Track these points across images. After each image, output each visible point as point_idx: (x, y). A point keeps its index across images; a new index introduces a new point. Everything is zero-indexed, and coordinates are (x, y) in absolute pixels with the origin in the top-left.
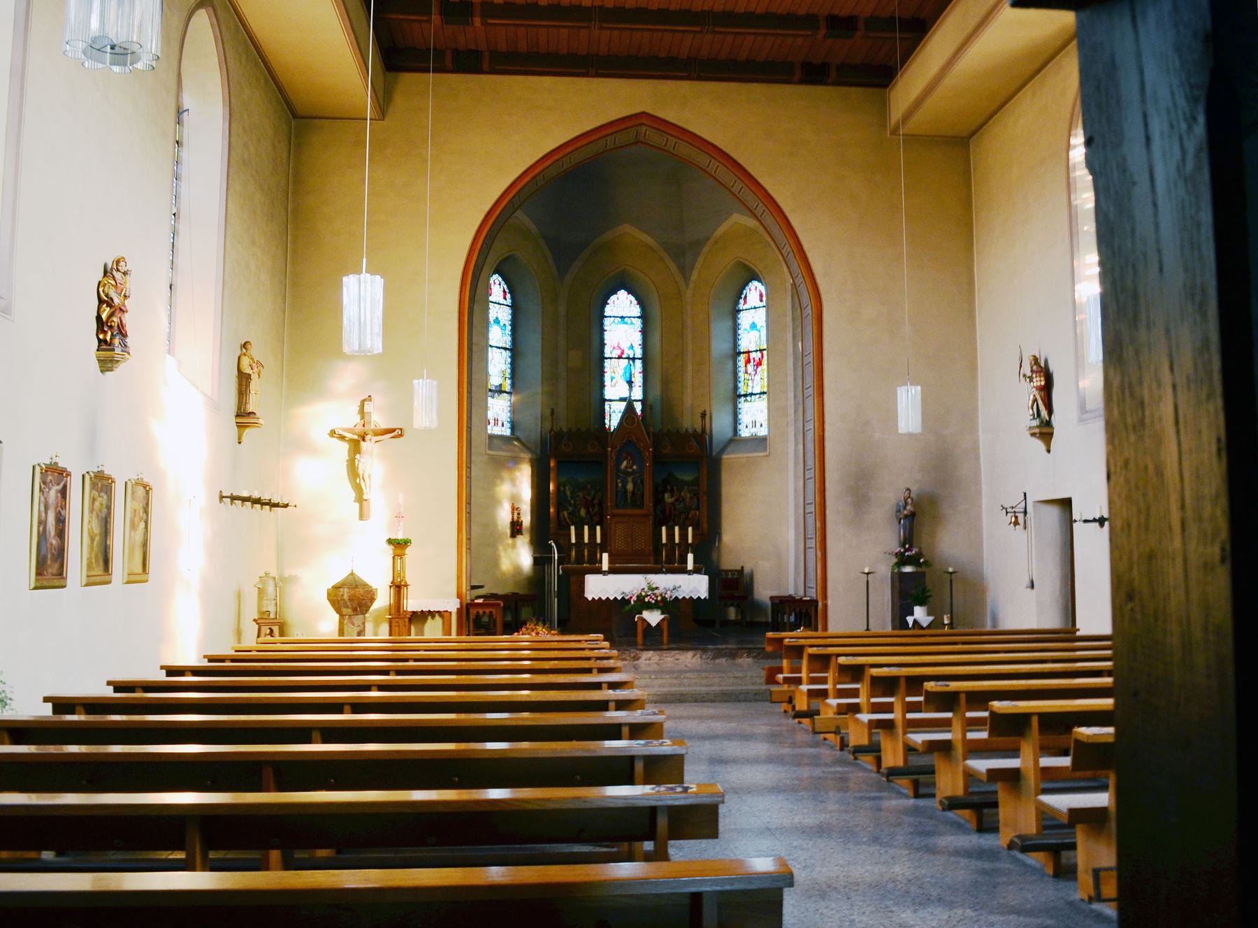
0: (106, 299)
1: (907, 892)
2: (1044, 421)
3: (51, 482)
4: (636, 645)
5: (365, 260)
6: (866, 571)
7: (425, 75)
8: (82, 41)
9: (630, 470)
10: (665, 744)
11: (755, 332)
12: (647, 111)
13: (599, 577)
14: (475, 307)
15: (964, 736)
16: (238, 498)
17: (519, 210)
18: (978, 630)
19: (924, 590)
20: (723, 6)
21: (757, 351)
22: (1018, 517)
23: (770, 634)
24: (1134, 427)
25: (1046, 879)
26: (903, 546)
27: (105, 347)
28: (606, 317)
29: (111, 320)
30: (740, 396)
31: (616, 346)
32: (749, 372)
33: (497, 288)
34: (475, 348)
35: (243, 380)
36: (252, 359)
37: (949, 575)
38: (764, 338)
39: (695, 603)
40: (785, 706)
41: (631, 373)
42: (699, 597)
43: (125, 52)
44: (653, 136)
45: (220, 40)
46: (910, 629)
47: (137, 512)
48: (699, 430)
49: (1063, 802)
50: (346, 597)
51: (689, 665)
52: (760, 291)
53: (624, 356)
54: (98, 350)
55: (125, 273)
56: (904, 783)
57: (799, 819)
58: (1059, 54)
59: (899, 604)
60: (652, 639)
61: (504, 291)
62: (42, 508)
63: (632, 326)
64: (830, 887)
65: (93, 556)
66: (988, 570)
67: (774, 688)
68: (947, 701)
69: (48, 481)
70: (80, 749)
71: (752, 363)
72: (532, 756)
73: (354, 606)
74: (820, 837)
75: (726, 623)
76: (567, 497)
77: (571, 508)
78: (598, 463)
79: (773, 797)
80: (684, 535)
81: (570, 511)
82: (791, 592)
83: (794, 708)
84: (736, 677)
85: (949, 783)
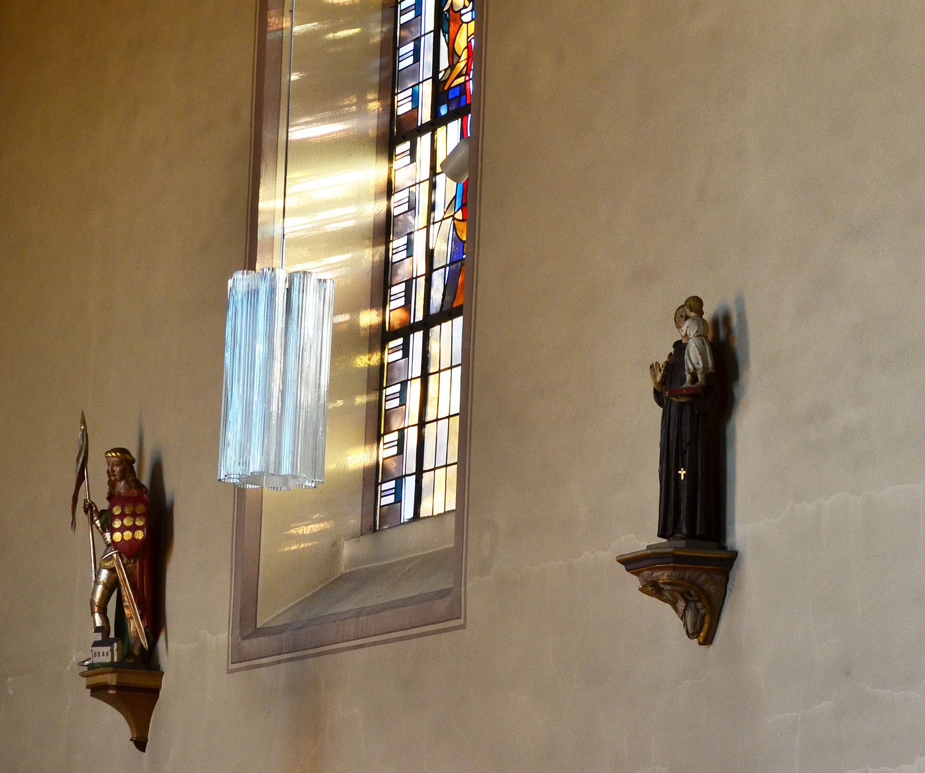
2: (136, 652)
58: (412, 598)
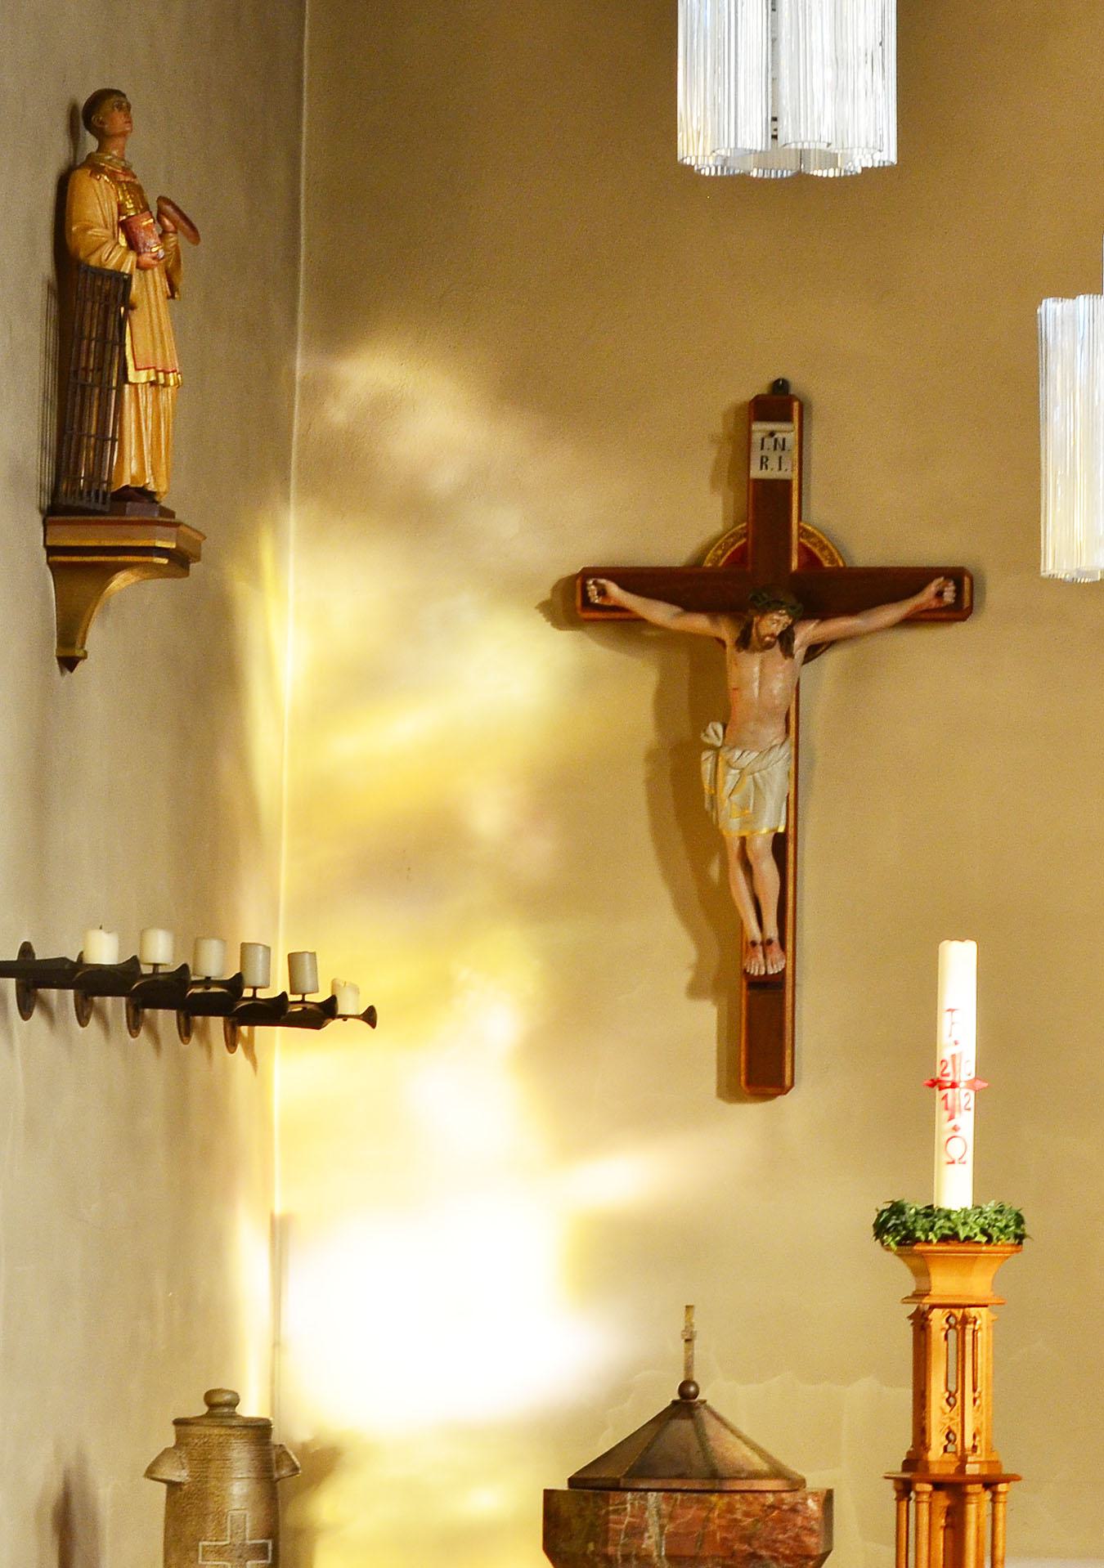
36: (136, 191)
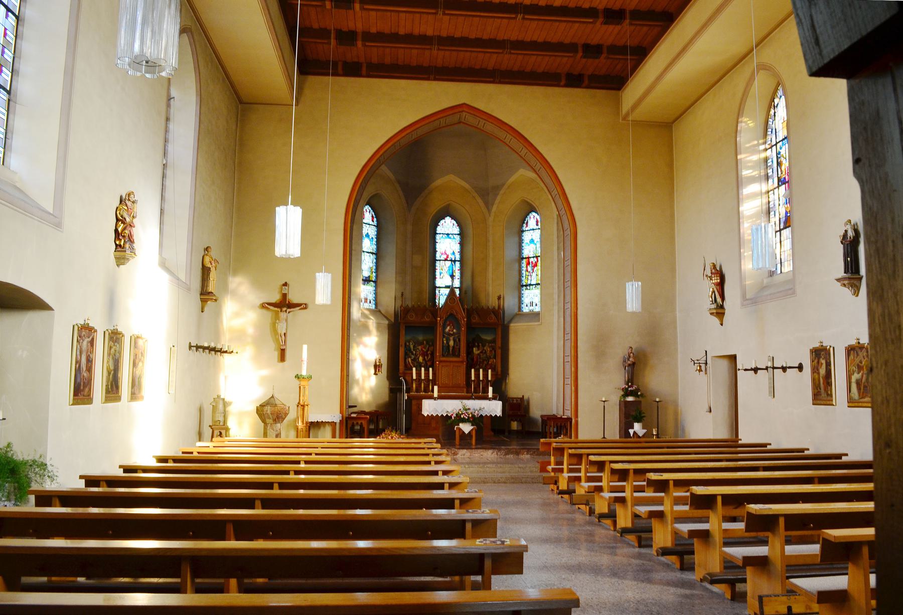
0: (121, 218)
1: (638, 609)
2: (719, 305)
3: (84, 336)
4: (455, 446)
5: (290, 196)
6: (604, 399)
7: (326, 78)
8: (128, 58)
9: (452, 333)
10: (485, 512)
11: (532, 246)
12: (468, 103)
13: (432, 401)
14: (354, 226)
15: (672, 508)
16: (201, 347)
17: (383, 165)
18: (679, 439)
19: (640, 413)
20: (516, 37)
21: (533, 257)
22: (702, 366)
23: (542, 440)
24: (892, 341)
25: (726, 601)
26: (628, 384)
27: (120, 249)
28: (437, 234)
29: (124, 232)
30: (523, 286)
31: (443, 252)
32: (529, 271)
33: (368, 215)
34: (353, 253)
35: (205, 272)
37: (656, 403)
38: (539, 250)
39: (493, 419)
40: (552, 486)
41: (453, 270)
42: (496, 415)
43: (155, 65)
44: (471, 119)
45: (195, 53)
46: (631, 437)
47: (137, 356)
48: (497, 308)
49: (739, 552)
50: (269, 412)
51: (490, 459)
52: (537, 219)
53: (448, 259)
54: (115, 251)
55: (133, 202)
56: (631, 538)
57: (565, 561)
59: (624, 421)
60: (465, 441)
61: (372, 217)
62: (78, 353)
63: (454, 240)
64: (588, 605)
65: (109, 384)
66: (681, 402)
67: (545, 475)
68: (662, 486)
69: (82, 335)
70: (99, 510)
71: (531, 265)
72: (401, 519)
73: (274, 418)
74: (579, 572)
75: (511, 432)
76: (411, 349)
77: (413, 357)
78: (431, 328)
79: (548, 546)
80: (485, 375)
81: (412, 358)
82: (555, 413)
83: (558, 488)
84: (520, 468)
85: (662, 537)
